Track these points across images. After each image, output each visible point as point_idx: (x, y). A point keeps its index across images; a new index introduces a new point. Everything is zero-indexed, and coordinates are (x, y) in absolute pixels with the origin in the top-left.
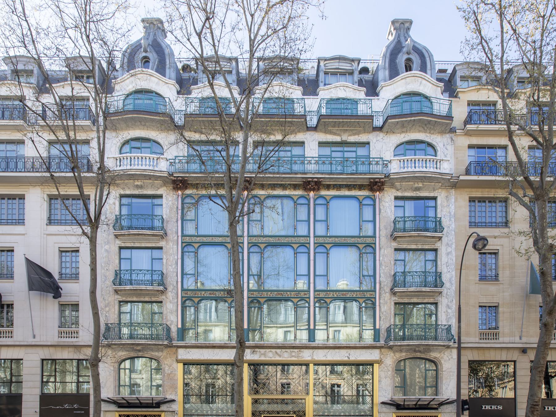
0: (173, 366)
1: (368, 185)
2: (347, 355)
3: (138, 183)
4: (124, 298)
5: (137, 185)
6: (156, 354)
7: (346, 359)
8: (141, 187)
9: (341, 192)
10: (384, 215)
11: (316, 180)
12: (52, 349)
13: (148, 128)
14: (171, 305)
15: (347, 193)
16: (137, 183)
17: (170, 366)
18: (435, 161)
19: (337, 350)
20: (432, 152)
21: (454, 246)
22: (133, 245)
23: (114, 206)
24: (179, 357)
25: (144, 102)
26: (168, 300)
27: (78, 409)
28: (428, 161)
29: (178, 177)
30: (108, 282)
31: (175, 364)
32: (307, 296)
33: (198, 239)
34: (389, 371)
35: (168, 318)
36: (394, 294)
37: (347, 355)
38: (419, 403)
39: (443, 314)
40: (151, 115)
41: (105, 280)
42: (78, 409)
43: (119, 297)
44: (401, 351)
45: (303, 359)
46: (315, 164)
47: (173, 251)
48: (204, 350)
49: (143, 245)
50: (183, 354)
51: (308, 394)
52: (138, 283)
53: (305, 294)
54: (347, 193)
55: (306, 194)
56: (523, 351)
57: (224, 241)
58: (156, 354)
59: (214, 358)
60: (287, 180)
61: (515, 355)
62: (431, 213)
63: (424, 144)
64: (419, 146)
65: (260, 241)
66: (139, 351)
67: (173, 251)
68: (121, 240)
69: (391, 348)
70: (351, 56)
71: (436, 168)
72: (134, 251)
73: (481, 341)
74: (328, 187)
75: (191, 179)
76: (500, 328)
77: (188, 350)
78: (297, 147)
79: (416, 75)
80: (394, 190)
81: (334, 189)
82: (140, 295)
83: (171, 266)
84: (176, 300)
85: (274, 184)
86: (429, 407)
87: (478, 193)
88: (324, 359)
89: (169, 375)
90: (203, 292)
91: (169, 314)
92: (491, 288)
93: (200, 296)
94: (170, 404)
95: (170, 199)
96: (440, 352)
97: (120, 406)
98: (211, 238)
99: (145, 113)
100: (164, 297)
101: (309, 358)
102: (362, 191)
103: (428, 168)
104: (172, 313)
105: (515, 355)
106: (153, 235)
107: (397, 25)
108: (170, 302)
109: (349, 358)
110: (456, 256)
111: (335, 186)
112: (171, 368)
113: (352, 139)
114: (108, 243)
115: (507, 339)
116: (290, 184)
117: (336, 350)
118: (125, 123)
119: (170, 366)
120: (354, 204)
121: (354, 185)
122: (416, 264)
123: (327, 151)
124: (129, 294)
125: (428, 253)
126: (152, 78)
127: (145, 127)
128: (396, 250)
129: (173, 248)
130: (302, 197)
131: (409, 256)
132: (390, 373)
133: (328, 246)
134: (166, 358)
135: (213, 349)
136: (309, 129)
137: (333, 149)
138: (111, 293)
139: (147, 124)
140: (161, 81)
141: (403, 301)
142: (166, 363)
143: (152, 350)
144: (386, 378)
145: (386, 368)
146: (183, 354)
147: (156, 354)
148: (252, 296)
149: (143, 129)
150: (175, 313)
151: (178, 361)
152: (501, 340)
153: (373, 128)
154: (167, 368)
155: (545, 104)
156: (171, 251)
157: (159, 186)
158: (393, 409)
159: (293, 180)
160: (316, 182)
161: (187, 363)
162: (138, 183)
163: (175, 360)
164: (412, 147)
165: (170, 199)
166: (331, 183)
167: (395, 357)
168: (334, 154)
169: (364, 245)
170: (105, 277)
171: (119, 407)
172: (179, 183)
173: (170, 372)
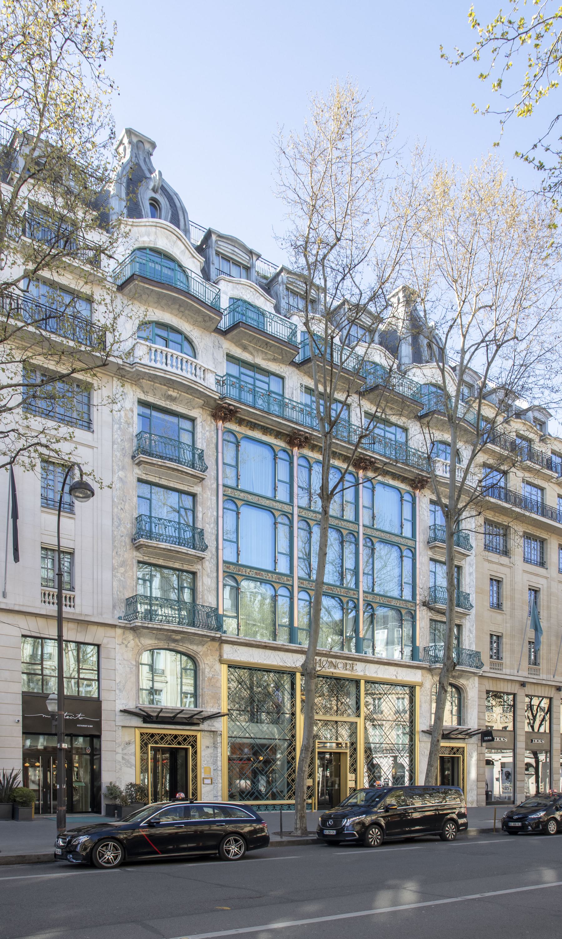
0: (215, 667)
1: (288, 435)
2: (395, 673)
3: (174, 394)
4: (147, 558)
5: (171, 396)
6: (193, 648)
7: (394, 678)
8: (172, 399)
10: (422, 517)
11: (373, 460)
12: (41, 621)
13: (195, 323)
14: (209, 580)
15: (391, 482)
16: (170, 393)
17: (211, 667)
18: (194, 364)
20: (190, 352)
21: (474, 567)
22: (157, 481)
23: (131, 413)
24: (225, 657)
25: (156, 268)
26: (205, 572)
27: (84, 722)
28: (159, 353)
29: (230, 405)
30: (123, 529)
31: (217, 665)
33: (242, 494)
35: (206, 598)
36: (138, 548)
37: (395, 673)
38: (160, 715)
39: (467, 638)
40: (208, 310)
41: (119, 525)
42: (84, 722)
43: (138, 554)
45: (357, 674)
47: (211, 504)
48: (254, 649)
49: (172, 485)
50: (231, 653)
51: (359, 716)
52: (159, 537)
54: (391, 482)
55: (289, 448)
56: (522, 685)
57: (271, 506)
58: (195, 648)
59: (265, 662)
60: (345, 449)
61: (515, 688)
62: (186, 438)
63: (180, 336)
64: (173, 336)
65: (237, 496)
66: (175, 641)
67: (211, 504)
68: (144, 469)
69: (134, 629)
70: (250, 246)
71: (166, 364)
72: (155, 489)
73: (530, 676)
74: (240, 422)
75: (242, 412)
76: (541, 665)
77: (235, 647)
78: (233, 365)
79: (168, 228)
80: (138, 390)
81: (246, 426)
82: (171, 558)
83: (209, 524)
84: (215, 574)
85: (256, 424)
86: (175, 720)
87: (531, 530)
88: (375, 675)
89: (210, 679)
90: (248, 570)
91: (206, 592)
92: (497, 617)
93: (244, 574)
94: (212, 720)
95: (207, 429)
96: (468, 679)
97: (147, 718)
98: (257, 497)
99: (195, 300)
100: (199, 567)
101: (361, 674)
102: (278, 440)
103: (169, 366)
104: (210, 592)
105: (515, 688)
106: (193, 476)
107: (147, 146)
108: (208, 576)
110: (476, 578)
111: (249, 424)
112: (213, 670)
113: (264, 364)
114: (123, 468)
115: (508, 671)
116: (340, 454)
118: (158, 298)
119: (211, 667)
120: (267, 454)
121: (400, 475)
122: (165, 506)
123: (234, 370)
124: (151, 553)
125: (184, 497)
126: (179, 242)
127: (181, 315)
128: (431, 559)
129: (211, 499)
130: (408, 492)
131: (158, 495)
133: (239, 503)
134: (206, 655)
135: (264, 650)
136: (293, 364)
137: (243, 370)
138: (128, 547)
139: (187, 312)
140: (187, 251)
142: (206, 662)
143: (192, 643)
146: (231, 653)
147: (193, 648)
149: (176, 315)
150: (215, 593)
151: (221, 661)
152: (504, 671)
153: (216, 328)
154: (207, 670)
155: (487, 420)
156: (209, 503)
157: (197, 406)
158: (137, 722)
159: (264, 420)
160: (231, 410)
161: (233, 666)
162: (174, 394)
163: (217, 659)
164: (164, 334)
165: (207, 429)
166: (246, 418)
168: (243, 377)
169: (244, 502)
170: (119, 519)
171: (145, 721)
172: (223, 412)
173: (211, 676)
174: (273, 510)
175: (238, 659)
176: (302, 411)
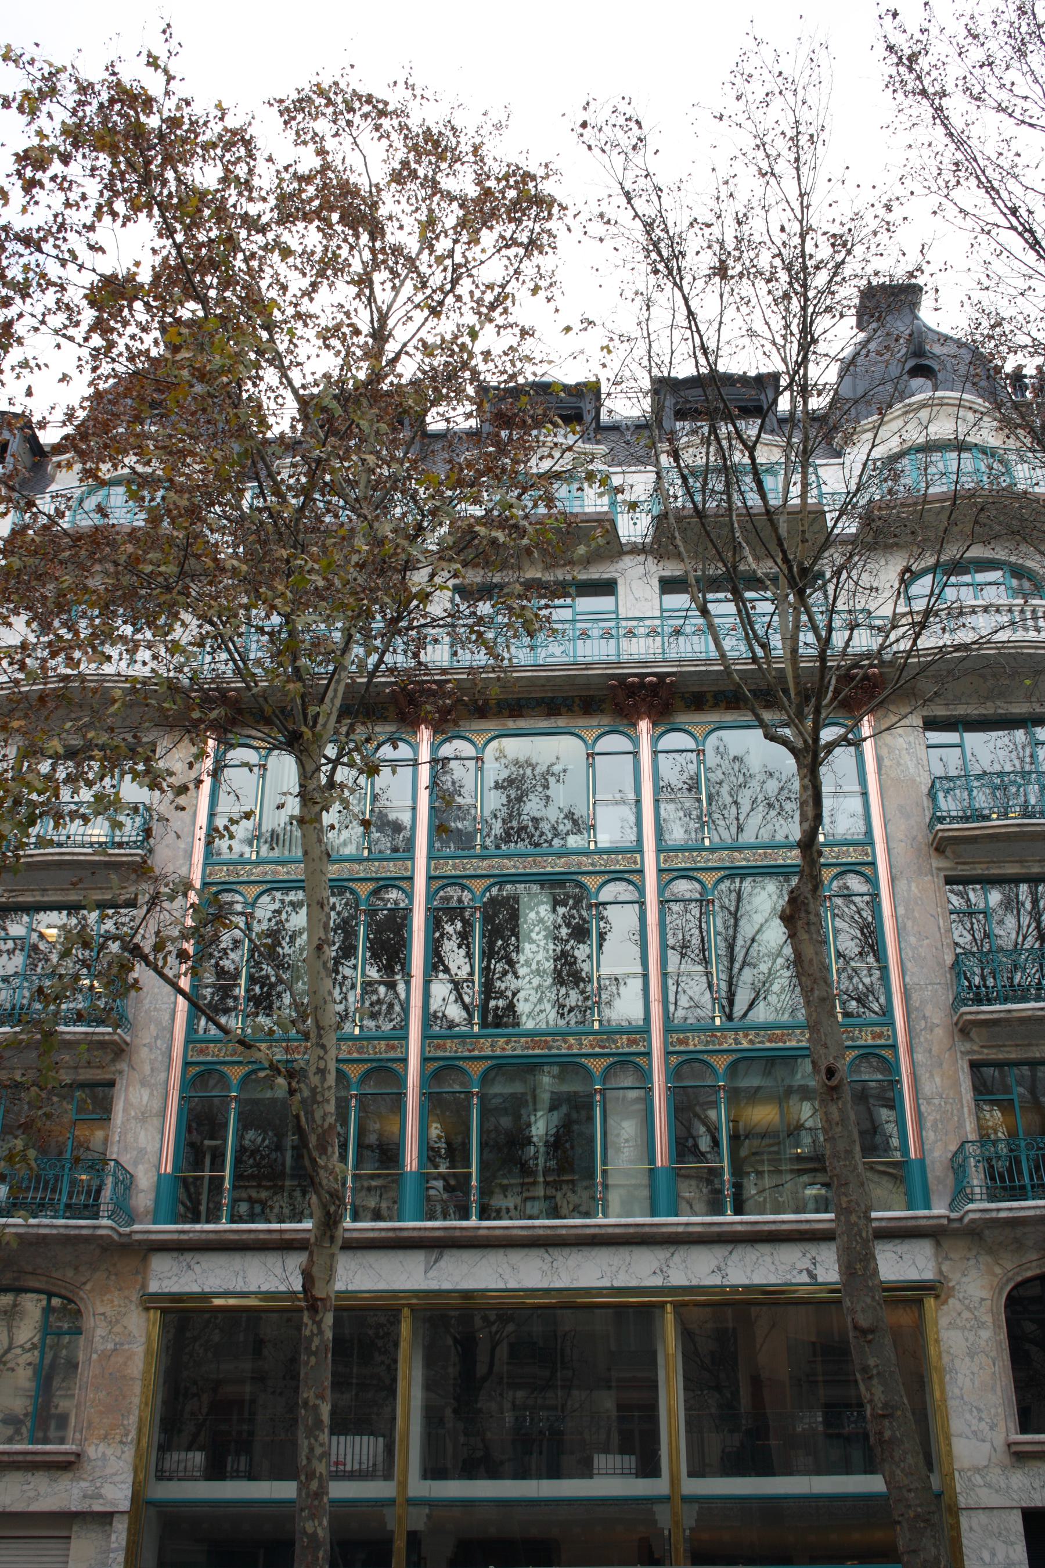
19: (765, 1249)
24: (153, 1287)
34: (982, 1325)
35: (130, 1137)
44: (1019, 1246)
46: (601, 637)
65: (471, 872)
88: (716, 1280)
89: (106, 1356)
109: (812, 1275)
117: (758, 1246)
132: (985, 1334)
144: (972, 1354)
145: (966, 1314)
148: (440, 1054)
154: (99, 1332)
167: (998, 1270)
174: (695, 874)
176: (653, 633)
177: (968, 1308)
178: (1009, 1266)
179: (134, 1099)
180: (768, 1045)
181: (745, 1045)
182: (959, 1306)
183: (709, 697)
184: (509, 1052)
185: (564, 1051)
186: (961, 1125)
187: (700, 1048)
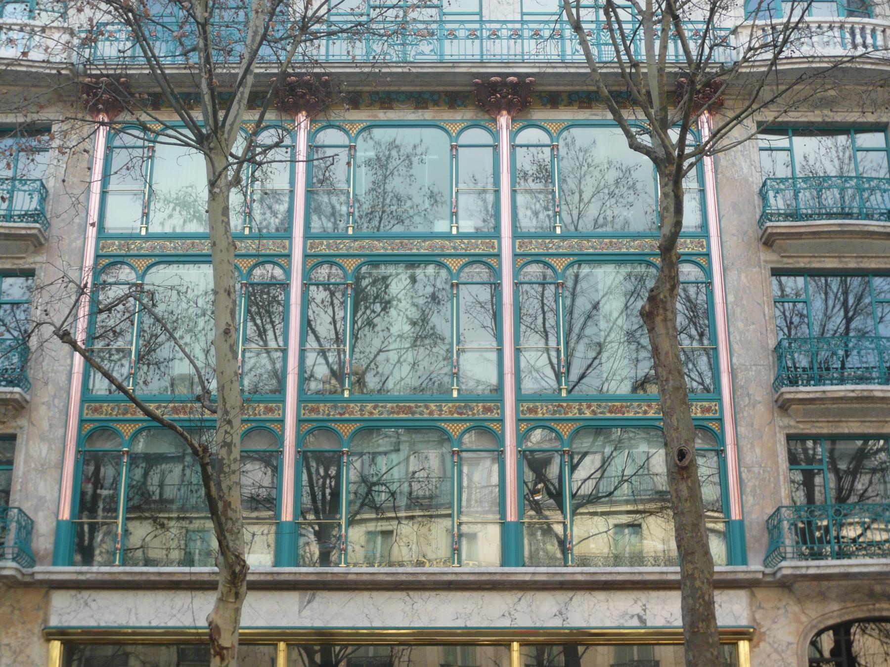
9: (594, 111)
19: (601, 596)
24: (54, 622)
32: (275, 416)
44: (823, 597)
53: (487, 410)
77: (85, 594)
88: (557, 623)
141: (814, 431)
145: (774, 656)
148: (314, 416)
167: (804, 619)
175: (92, 623)
176: (536, 34)
177: (776, 651)
178: (813, 615)
179: (34, 453)
180: (608, 415)
181: (588, 414)
182: (768, 649)
183: (564, 96)
184: (376, 416)
185: (426, 416)
186: (776, 491)
187: (547, 416)
